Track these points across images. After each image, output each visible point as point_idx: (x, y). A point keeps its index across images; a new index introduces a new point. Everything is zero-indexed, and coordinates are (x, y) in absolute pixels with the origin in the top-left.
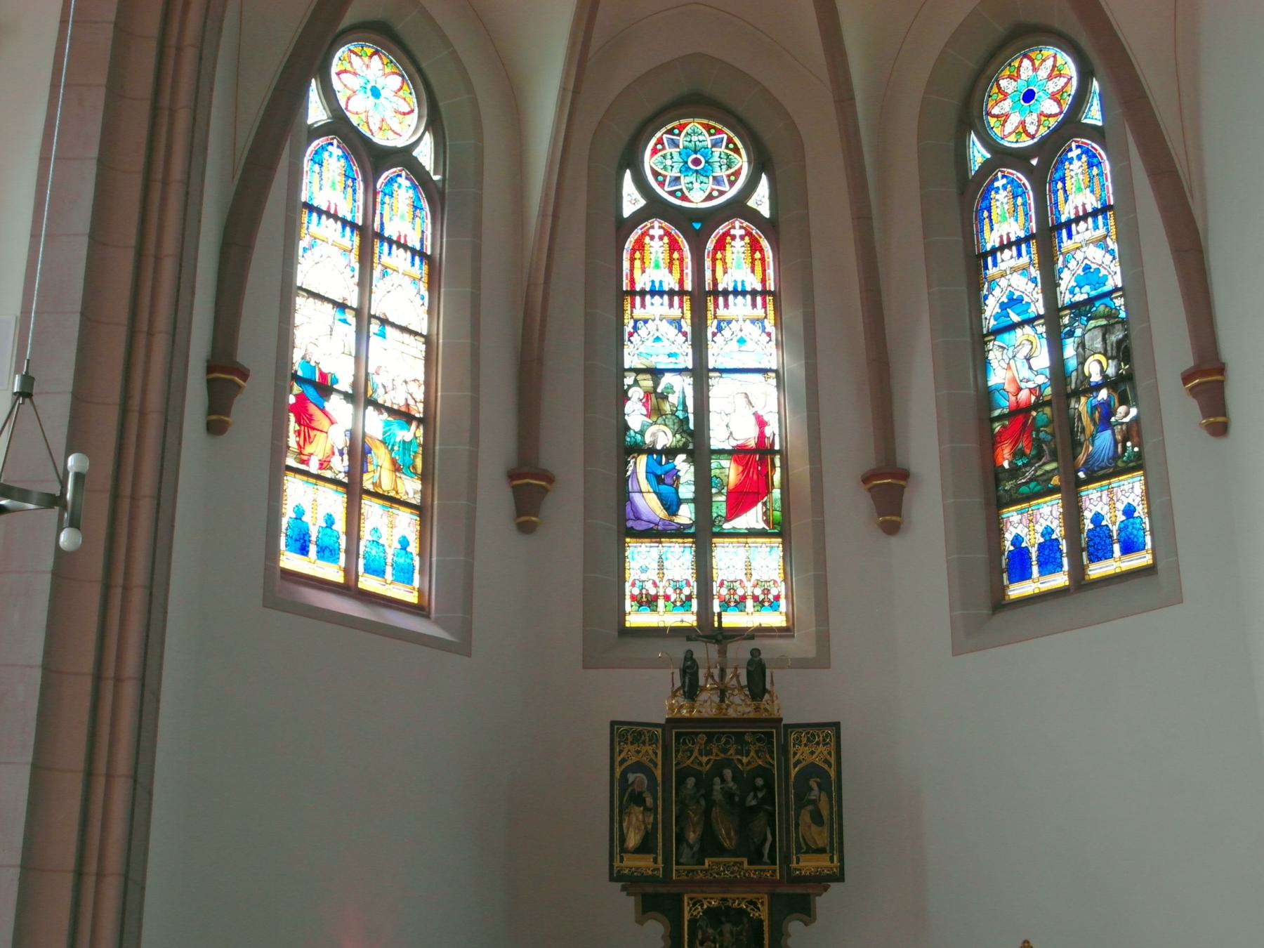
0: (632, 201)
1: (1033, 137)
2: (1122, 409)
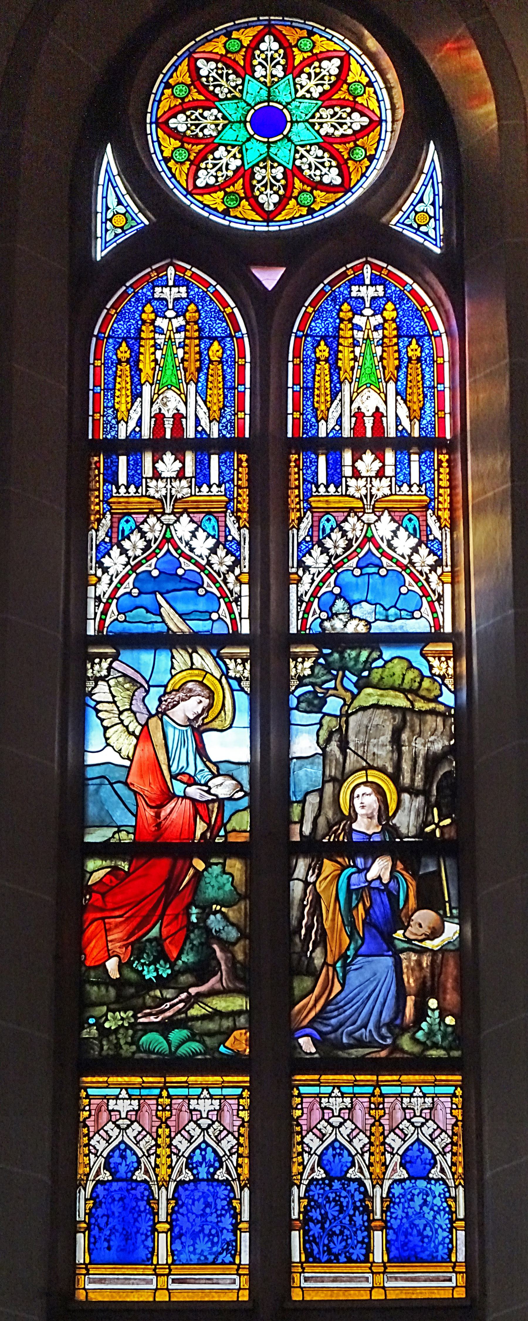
1: (268, 217)
2: (425, 918)
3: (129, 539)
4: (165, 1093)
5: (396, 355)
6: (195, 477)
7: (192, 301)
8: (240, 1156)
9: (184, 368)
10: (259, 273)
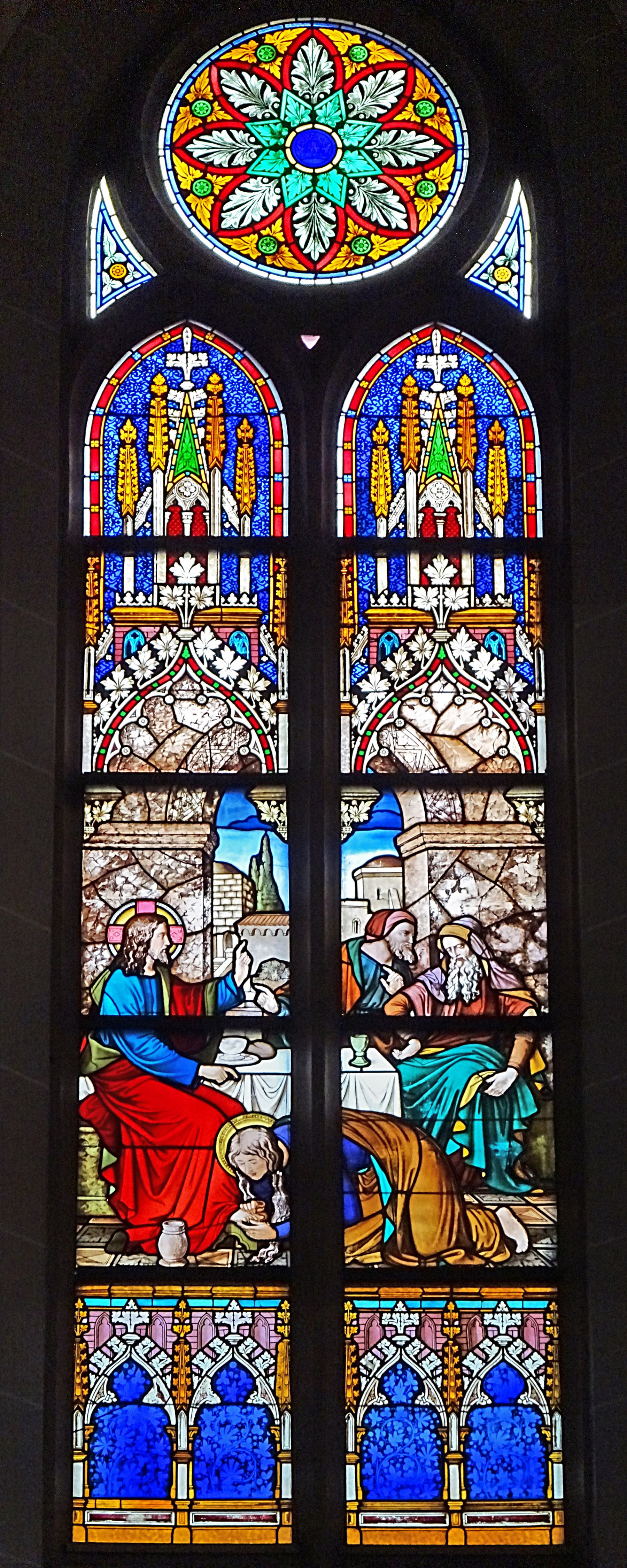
0: (113, 263)
3: (137, 657)
4: (182, 1305)
5: (474, 440)
6: (220, 584)
7: (464, 372)
8: (548, 1377)
9: (457, 453)
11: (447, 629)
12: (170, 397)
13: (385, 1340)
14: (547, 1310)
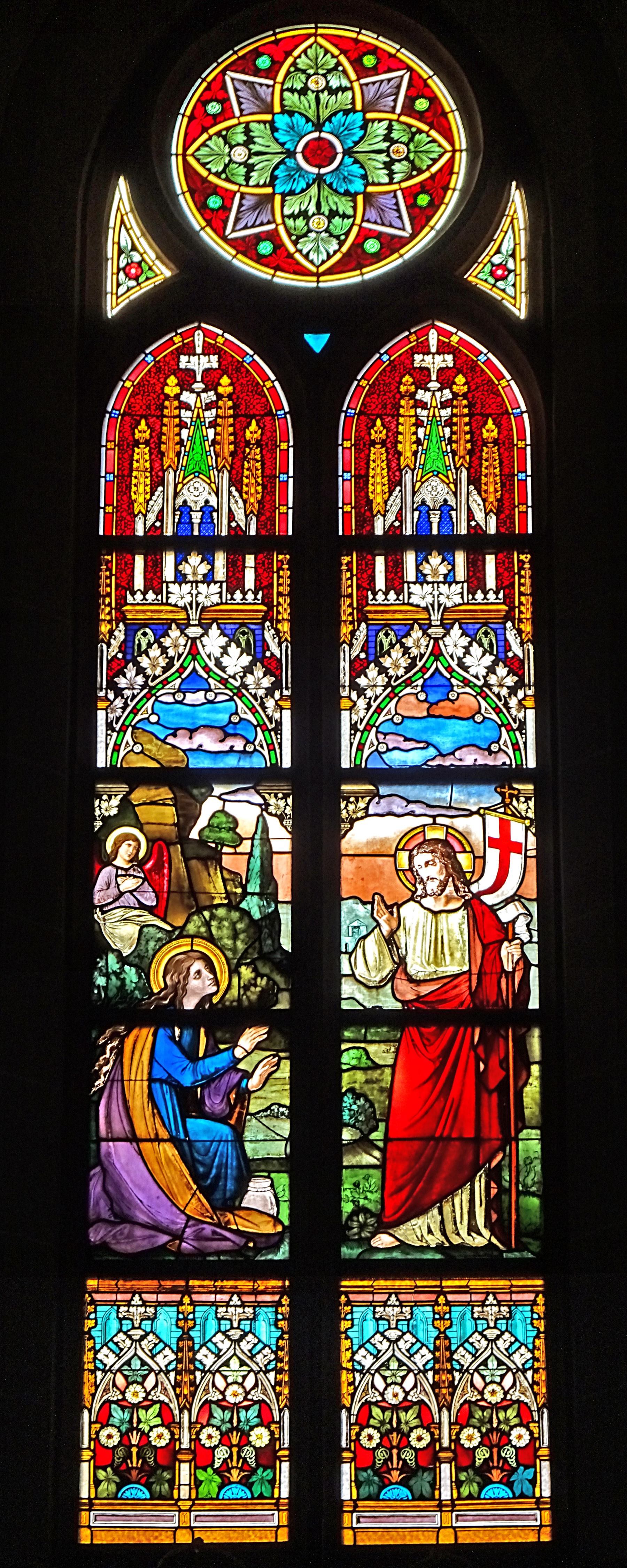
0: (130, 264)
4: (186, 1300)
8: (279, 1371)
10: (308, 338)
11: (200, 625)
12: (418, 397)
13: (121, 1334)
14: (279, 1304)
